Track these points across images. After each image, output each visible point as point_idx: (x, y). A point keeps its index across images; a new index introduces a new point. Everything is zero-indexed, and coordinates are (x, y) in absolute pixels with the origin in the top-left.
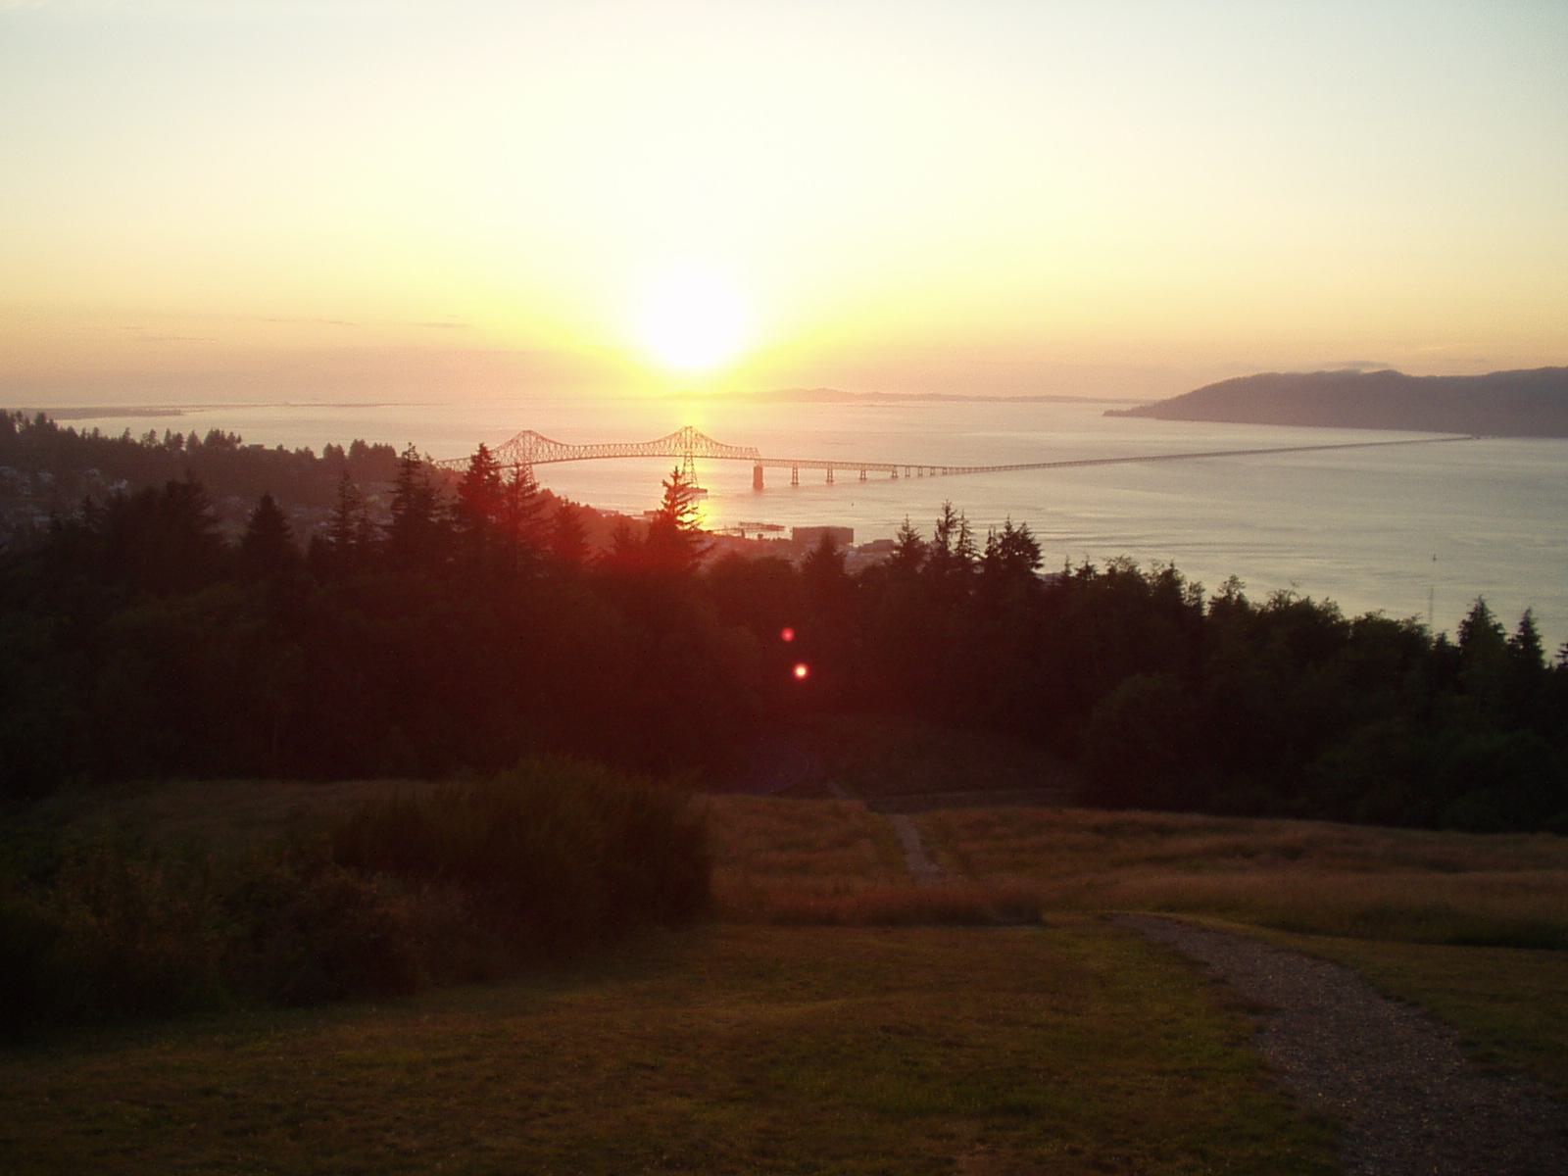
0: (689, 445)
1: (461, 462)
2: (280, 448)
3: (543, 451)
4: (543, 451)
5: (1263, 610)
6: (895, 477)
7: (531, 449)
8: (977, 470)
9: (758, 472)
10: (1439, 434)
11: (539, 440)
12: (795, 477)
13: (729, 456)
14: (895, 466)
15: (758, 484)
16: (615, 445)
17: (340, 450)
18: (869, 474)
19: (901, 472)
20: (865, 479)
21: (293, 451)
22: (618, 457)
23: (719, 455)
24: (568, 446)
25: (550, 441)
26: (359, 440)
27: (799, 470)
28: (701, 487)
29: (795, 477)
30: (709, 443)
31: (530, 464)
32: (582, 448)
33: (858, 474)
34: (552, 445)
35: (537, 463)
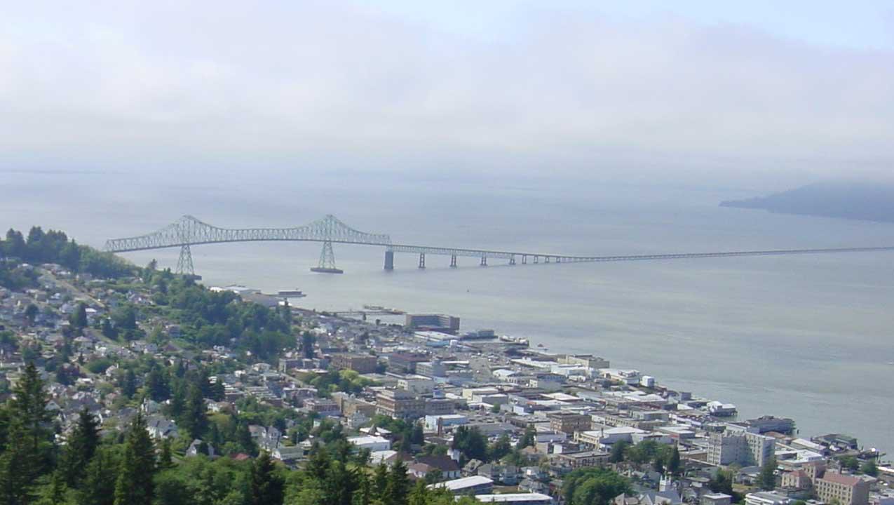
0: (328, 231)
1: (140, 240)
2: (39, 228)
3: (200, 233)
4: (200, 233)
5: (282, 478)
6: (512, 264)
7: (189, 232)
8: (795, 252)
9: (389, 256)
10: (543, 404)
11: (197, 224)
12: (422, 262)
13: (364, 241)
14: (513, 254)
15: (389, 266)
16: (273, 230)
17: (19, 235)
18: (489, 261)
19: (518, 259)
20: (485, 264)
21: (46, 232)
22: (229, 241)
23: (355, 241)
24: (278, 230)
25: (206, 225)
26: (37, 226)
27: (426, 256)
28: (337, 268)
29: (422, 262)
30: (346, 230)
31: (188, 244)
32: (235, 232)
33: (447, 259)
34: (208, 230)
35: (334, 241)
